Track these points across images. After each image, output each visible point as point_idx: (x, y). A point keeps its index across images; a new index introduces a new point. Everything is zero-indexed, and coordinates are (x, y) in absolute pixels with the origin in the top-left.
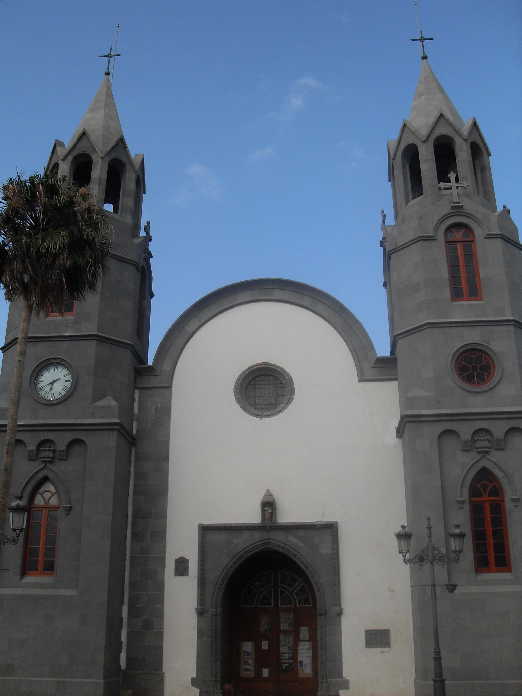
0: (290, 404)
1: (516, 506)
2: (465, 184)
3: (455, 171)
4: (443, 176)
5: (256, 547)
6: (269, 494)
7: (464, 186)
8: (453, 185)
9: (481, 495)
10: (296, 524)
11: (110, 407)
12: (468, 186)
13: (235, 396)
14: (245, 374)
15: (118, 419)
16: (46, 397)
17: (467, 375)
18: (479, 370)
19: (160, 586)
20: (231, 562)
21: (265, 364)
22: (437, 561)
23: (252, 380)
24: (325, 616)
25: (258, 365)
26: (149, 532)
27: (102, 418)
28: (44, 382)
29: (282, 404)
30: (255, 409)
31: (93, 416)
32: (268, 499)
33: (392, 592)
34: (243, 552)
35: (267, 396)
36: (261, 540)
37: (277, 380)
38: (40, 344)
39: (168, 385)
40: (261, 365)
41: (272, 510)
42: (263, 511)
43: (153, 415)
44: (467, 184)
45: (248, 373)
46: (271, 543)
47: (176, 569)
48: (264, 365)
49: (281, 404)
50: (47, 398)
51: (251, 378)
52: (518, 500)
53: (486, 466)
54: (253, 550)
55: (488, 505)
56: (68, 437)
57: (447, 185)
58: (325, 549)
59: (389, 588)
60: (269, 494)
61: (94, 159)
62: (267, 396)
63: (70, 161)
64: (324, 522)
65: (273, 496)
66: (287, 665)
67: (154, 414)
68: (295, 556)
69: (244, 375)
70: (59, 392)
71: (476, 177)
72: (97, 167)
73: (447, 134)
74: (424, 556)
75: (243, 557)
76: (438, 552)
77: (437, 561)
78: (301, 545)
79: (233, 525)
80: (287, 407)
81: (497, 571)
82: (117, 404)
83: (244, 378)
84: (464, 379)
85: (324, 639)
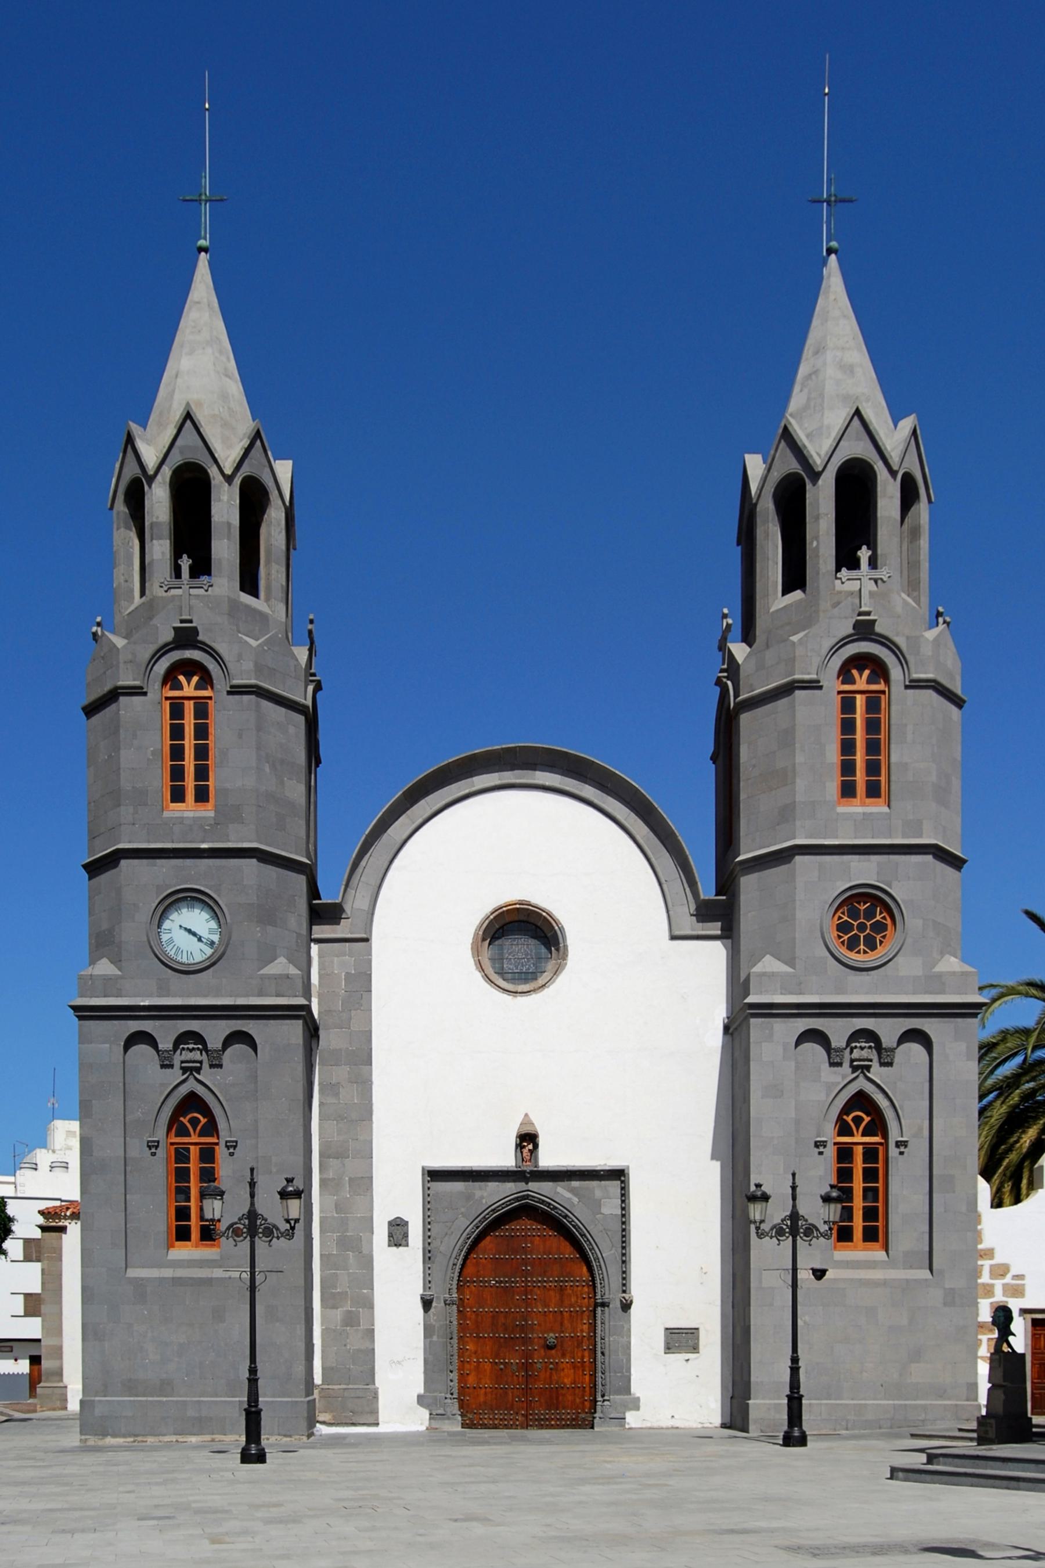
0: (560, 973)
1: (902, 1153)
2: (885, 573)
3: (872, 546)
4: (847, 560)
5: (508, 1203)
6: (527, 1120)
7: (882, 577)
8: (863, 576)
9: (851, 1134)
10: (569, 1169)
11: (288, 977)
12: (889, 577)
13: (473, 957)
14: (489, 919)
15: (302, 999)
16: (179, 958)
17: (848, 938)
18: (862, 920)
19: (367, 1263)
20: (472, 1225)
21: (521, 903)
22: (802, 1235)
23: (499, 929)
24: (608, 1306)
25: (510, 905)
26: (347, 1178)
27: (276, 996)
28: (173, 931)
29: (546, 973)
30: (504, 980)
31: (260, 994)
32: (527, 1129)
33: (705, 1273)
34: (490, 1209)
35: (522, 959)
36: (515, 1192)
37: (538, 930)
38: (159, 862)
39: (364, 936)
40: (515, 904)
41: (533, 1146)
42: (519, 1147)
43: (343, 987)
44: (888, 573)
45: (495, 918)
46: (530, 1198)
47: (391, 1235)
48: (520, 904)
49: (544, 972)
50: (181, 960)
51: (497, 927)
52: (905, 1144)
53: (864, 1089)
54: (503, 1208)
55: (859, 1151)
56: (226, 1027)
57: (854, 574)
58: (611, 1207)
59: (702, 1268)
60: (527, 1120)
61: (214, 479)
62: (522, 959)
63: (168, 480)
64: (609, 1166)
65: (533, 1124)
66: (1010, 1351)
67: (345, 986)
68: (566, 1217)
69: (487, 922)
70: (201, 950)
71: (901, 547)
72: (222, 498)
73: (864, 457)
74: (785, 1227)
75: (489, 1218)
76: (804, 1223)
77: (802, 1235)
78: (575, 1200)
79: (474, 1169)
80: (556, 978)
81: (864, 1249)
82: (300, 972)
83: (487, 926)
84: (844, 945)
85: (606, 1339)
